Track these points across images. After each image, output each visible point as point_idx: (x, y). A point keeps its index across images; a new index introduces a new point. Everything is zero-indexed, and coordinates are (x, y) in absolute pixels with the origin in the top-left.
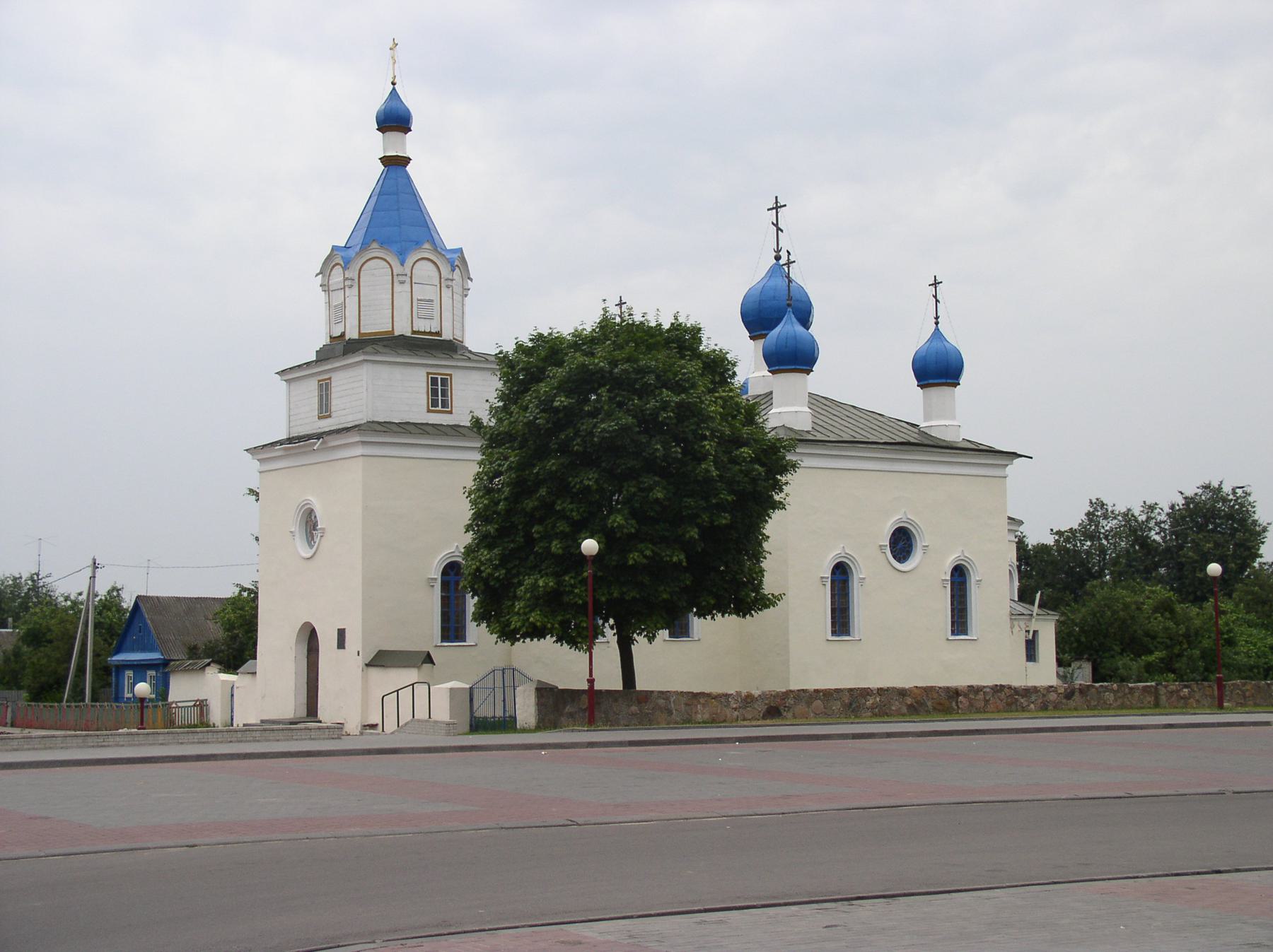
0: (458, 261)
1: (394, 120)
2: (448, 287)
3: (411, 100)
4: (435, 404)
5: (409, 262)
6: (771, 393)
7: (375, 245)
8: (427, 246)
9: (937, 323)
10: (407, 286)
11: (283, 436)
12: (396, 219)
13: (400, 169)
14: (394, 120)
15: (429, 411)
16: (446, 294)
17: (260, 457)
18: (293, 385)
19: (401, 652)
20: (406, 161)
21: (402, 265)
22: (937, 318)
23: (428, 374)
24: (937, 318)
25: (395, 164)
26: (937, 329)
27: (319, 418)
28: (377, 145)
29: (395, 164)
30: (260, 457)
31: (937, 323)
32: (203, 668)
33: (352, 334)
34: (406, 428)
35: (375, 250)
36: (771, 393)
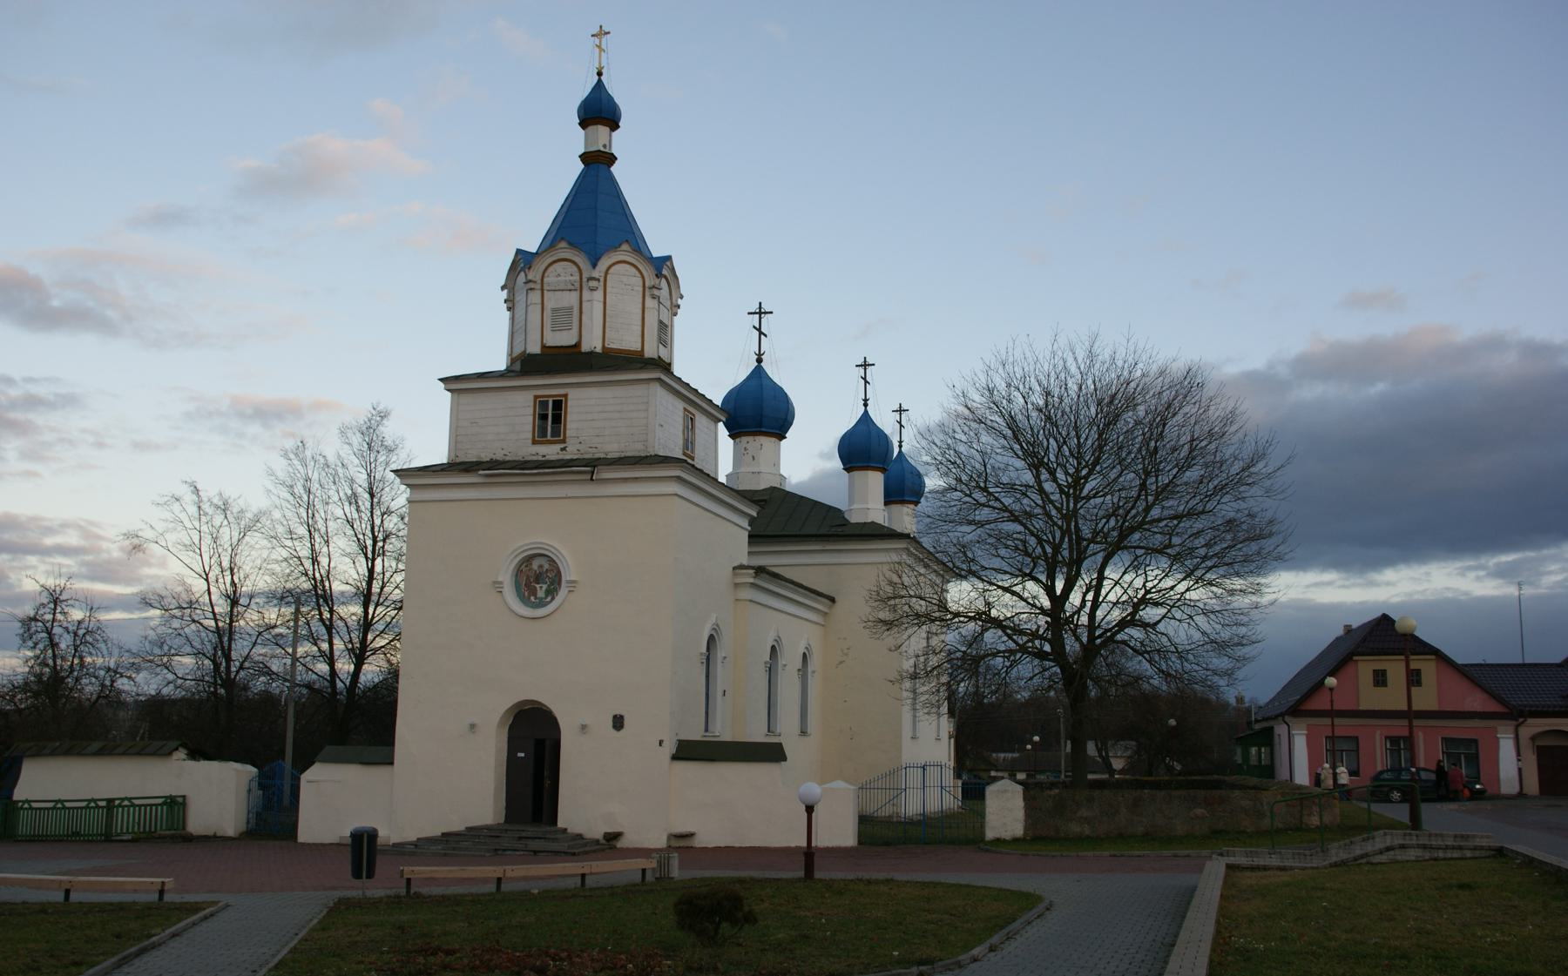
0: (662, 266)
1: (599, 111)
2: (653, 297)
3: (617, 91)
4: (543, 432)
5: (604, 264)
6: (675, 758)
7: (563, 244)
8: (625, 247)
9: (866, 405)
10: (599, 295)
11: (440, 456)
12: (593, 218)
13: (603, 167)
14: (599, 111)
15: (534, 442)
16: (650, 303)
17: (410, 481)
18: (466, 399)
19: (323, 845)
20: (612, 159)
21: (594, 266)
22: (866, 400)
23: (536, 397)
24: (866, 400)
25: (598, 162)
26: (866, 412)
27: (534, 442)
28: (576, 141)
29: (598, 162)
30: (410, 481)
31: (866, 405)
32: (170, 754)
33: (592, 343)
34: (523, 465)
35: (564, 250)
36: (675, 758)
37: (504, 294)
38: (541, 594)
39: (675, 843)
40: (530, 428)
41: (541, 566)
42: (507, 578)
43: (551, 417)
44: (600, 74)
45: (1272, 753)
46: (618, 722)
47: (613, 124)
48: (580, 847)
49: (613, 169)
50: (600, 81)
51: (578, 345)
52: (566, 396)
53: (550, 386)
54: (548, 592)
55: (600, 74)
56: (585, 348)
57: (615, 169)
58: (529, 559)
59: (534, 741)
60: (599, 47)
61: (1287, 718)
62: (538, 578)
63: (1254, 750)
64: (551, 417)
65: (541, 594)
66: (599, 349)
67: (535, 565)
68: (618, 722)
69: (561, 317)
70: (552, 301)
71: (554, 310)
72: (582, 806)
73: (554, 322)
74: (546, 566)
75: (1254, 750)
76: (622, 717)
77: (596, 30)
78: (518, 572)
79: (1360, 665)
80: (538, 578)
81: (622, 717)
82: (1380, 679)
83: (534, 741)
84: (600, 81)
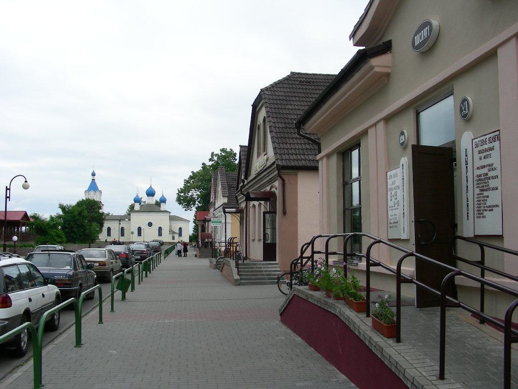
25: (93, 180)
29: (93, 180)
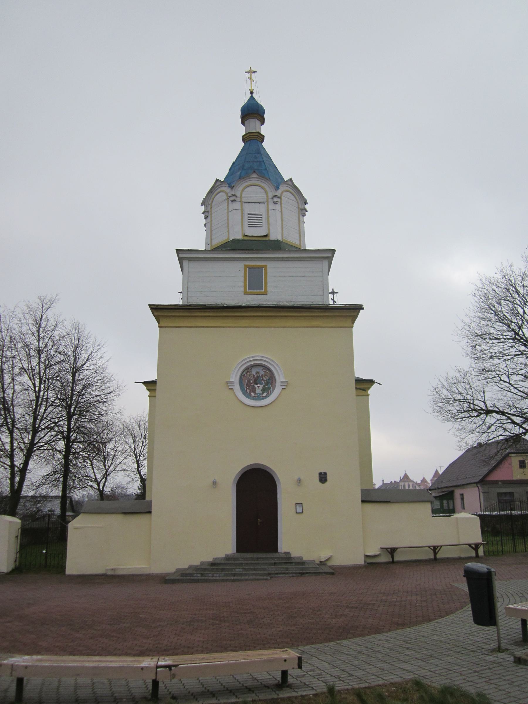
1: (252, 112)
11: (177, 300)
13: (259, 143)
14: (252, 112)
15: (246, 293)
20: (262, 138)
23: (246, 266)
25: (253, 140)
29: (253, 140)
37: (202, 209)
38: (259, 391)
39: (369, 561)
40: (242, 284)
41: (258, 373)
42: (235, 378)
43: (255, 280)
44: (252, 93)
45: (453, 503)
46: (323, 478)
47: (263, 123)
48: (301, 569)
49: (264, 144)
50: (252, 96)
51: (266, 236)
52: (265, 267)
53: (256, 260)
54: (264, 390)
55: (252, 93)
56: (272, 237)
57: (265, 144)
58: (248, 369)
59: (256, 492)
60: (250, 78)
61: (479, 485)
62: (257, 380)
63: (445, 502)
64: (255, 280)
65: (259, 391)
66: (239, 237)
67: (254, 372)
68: (323, 478)
69: (255, 220)
70: (249, 209)
71: (249, 214)
72: (293, 537)
73: (249, 220)
74: (262, 373)
75: (445, 502)
76: (325, 474)
77: (248, 70)
78: (242, 376)
79: (512, 458)
80: (257, 380)
81: (325, 474)
82: (522, 465)
83: (256, 492)
84: (252, 96)
